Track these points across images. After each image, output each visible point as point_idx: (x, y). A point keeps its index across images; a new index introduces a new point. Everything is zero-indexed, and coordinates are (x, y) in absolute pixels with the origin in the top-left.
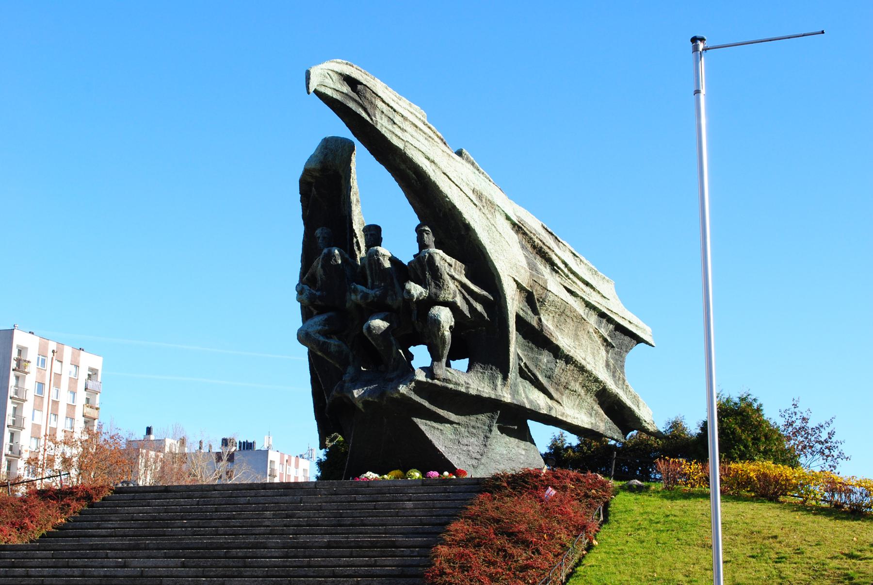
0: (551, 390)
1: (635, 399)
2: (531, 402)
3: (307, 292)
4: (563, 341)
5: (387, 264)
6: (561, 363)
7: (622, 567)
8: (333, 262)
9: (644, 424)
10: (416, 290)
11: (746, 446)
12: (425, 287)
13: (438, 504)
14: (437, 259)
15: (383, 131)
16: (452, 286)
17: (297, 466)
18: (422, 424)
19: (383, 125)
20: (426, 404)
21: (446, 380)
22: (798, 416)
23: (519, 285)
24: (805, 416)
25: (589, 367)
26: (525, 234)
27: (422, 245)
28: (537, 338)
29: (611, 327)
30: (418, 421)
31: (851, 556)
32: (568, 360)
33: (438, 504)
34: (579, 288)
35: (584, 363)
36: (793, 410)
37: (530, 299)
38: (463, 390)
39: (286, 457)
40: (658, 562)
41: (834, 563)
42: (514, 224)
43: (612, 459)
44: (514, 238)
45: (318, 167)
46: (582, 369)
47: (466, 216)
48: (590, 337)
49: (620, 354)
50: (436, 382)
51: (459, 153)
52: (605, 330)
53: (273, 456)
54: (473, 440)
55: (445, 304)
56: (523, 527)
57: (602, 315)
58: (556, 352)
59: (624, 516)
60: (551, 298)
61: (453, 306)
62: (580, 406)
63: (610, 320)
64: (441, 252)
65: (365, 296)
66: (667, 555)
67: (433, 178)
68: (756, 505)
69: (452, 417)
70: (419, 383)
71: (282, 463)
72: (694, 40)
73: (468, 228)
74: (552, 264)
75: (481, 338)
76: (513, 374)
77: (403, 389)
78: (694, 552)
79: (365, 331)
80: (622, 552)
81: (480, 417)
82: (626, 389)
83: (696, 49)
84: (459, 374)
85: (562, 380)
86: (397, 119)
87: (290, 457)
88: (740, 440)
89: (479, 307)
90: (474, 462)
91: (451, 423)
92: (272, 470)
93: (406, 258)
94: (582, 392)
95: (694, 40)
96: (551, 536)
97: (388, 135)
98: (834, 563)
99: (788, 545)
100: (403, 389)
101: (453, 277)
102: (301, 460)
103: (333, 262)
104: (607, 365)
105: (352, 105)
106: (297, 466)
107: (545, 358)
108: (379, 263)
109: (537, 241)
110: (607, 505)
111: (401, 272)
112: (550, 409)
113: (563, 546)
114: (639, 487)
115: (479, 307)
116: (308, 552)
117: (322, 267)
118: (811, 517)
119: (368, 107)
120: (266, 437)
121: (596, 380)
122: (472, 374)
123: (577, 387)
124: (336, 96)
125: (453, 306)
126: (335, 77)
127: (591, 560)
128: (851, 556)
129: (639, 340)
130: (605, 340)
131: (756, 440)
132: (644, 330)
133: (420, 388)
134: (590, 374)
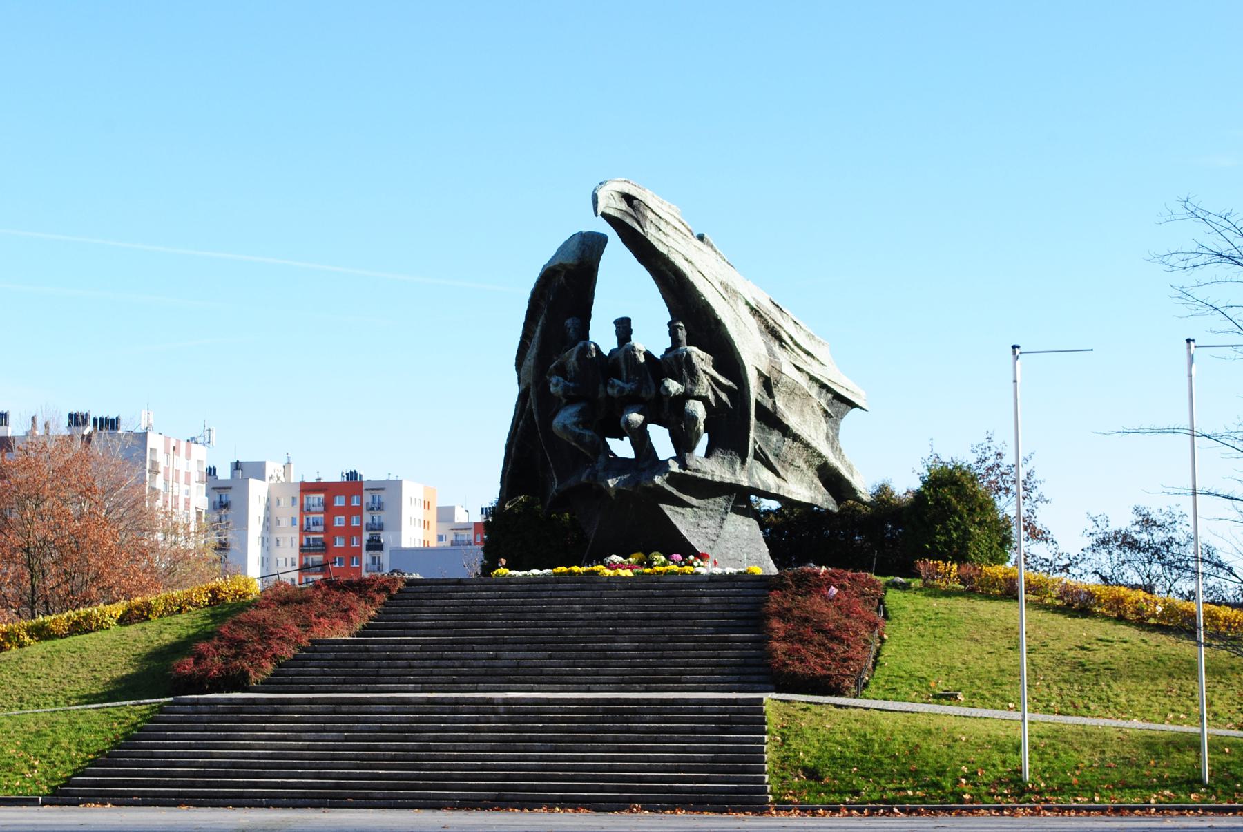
0: (779, 468)
1: (850, 468)
2: (763, 482)
3: (561, 384)
4: (792, 420)
5: (642, 359)
6: (788, 441)
7: (913, 657)
8: (588, 356)
9: (859, 494)
10: (674, 386)
11: (961, 518)
12: (681, 383)
13: (732, 599)
14: (694, 356)
15: (653, 240)
16: (705, 380)
17: (188, 456)
18: (668, 510)
19: (652, 235)
20: (674, 491)
21: (697, 470)
22: (993, 452)
23: (760, 373)
24: (999, 451)
25: (814, 444)
26: (761, 316)
27: (676, 341)
28: (771, 420)
29: (830, 396)
30: (663, 506)
31: (1083, 648)
32: (796, 438)
33: (732, 599)
34: (804, 360)
35: (809, 440)
36: (987, 444)
37: (768, 384)
38: (709, 478)
39: (173, 443)
40: (940, 653)
41: (1071, 654)
42: (752, 309)
43: (872, 558)
44: (753, 322)
45: (576, 262)
46: (807, 446)
47: (718, 312)
48: (814, 412)
49: (836, 423)
50: (688, 472)
51: (701, 238)
52: (823, 400)
53: (154, 441)
54: (710, 522)
55: (699, 398)
56: (832, 626)
57: (823, 386)
58: (785, 431)
59: (901, 613)
60: (784, 379)
61: (704, 400)
62: (802, 481)
63: (829, 390)
64: (695, 349)
65: (622, 389)
66: (945, 647)
67: (691, 279)
68: (1006, 604)
69: (694, 501)
70: (673, 474)
71: (167, 452)
72: (1014, 347)
73: (719, 323)
74: (780, 340)
75: (729, 430)
76: (750, 459)
77: (658, 480)
78: (966, 645)
79: (622, 424)
80: (909, 645)
81: (718, 500)
82: (841, 457)
83: (1014, 353)
84: (707, 464)
85: (789, 457)
86: (662, 225)
87: (178, 442)
88: (955, 512)
89: (724, 397)
90: (711, 544)
91: (692, 506)
92: (154, 463)
93: (658, 353)
94: (804, 467)
95: (1014, 347)
96: (856, 634)
97: (656, 243)
98: (1071, 654)
99: (1035, 639)
100: (658, 480)
101: (705, 372)
102: (193, 445)
103: (588, 356)
104: (827, 437)
105: (629, 221)
106: (188, 456)
107: (775, 437)
108: (635, 358)
109: (770, 321)
110: (881, 602)
111: (657, 368)
112: (779, 487)
113: (866, 641)
114: (902, 584)
115: (724, 397)
116: (656, 646)
117: (577, 359)
118: (1051, 615)
119: (641, 219)
120: (144, 412)
121: (819, 455)
122: (713, 459)
123: (800, 462)
124: (617, 214)
125: (704, 400)
126: (617, 196)
127: (886, 652)
128: (1083, 648)
129: (852, 405)
130: (826, 412)
131: (971, 511)
132: (859, 396)
133: (674, 479)
134: (814, 450)
